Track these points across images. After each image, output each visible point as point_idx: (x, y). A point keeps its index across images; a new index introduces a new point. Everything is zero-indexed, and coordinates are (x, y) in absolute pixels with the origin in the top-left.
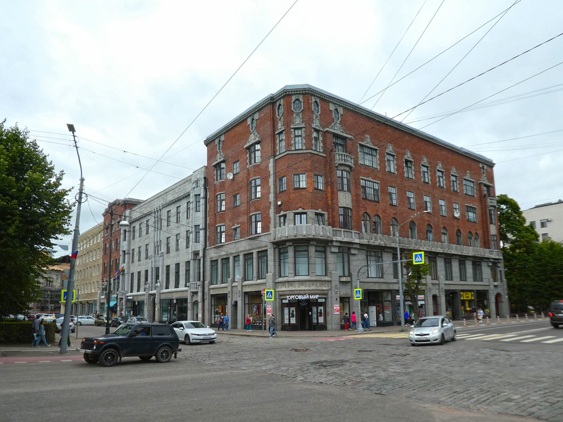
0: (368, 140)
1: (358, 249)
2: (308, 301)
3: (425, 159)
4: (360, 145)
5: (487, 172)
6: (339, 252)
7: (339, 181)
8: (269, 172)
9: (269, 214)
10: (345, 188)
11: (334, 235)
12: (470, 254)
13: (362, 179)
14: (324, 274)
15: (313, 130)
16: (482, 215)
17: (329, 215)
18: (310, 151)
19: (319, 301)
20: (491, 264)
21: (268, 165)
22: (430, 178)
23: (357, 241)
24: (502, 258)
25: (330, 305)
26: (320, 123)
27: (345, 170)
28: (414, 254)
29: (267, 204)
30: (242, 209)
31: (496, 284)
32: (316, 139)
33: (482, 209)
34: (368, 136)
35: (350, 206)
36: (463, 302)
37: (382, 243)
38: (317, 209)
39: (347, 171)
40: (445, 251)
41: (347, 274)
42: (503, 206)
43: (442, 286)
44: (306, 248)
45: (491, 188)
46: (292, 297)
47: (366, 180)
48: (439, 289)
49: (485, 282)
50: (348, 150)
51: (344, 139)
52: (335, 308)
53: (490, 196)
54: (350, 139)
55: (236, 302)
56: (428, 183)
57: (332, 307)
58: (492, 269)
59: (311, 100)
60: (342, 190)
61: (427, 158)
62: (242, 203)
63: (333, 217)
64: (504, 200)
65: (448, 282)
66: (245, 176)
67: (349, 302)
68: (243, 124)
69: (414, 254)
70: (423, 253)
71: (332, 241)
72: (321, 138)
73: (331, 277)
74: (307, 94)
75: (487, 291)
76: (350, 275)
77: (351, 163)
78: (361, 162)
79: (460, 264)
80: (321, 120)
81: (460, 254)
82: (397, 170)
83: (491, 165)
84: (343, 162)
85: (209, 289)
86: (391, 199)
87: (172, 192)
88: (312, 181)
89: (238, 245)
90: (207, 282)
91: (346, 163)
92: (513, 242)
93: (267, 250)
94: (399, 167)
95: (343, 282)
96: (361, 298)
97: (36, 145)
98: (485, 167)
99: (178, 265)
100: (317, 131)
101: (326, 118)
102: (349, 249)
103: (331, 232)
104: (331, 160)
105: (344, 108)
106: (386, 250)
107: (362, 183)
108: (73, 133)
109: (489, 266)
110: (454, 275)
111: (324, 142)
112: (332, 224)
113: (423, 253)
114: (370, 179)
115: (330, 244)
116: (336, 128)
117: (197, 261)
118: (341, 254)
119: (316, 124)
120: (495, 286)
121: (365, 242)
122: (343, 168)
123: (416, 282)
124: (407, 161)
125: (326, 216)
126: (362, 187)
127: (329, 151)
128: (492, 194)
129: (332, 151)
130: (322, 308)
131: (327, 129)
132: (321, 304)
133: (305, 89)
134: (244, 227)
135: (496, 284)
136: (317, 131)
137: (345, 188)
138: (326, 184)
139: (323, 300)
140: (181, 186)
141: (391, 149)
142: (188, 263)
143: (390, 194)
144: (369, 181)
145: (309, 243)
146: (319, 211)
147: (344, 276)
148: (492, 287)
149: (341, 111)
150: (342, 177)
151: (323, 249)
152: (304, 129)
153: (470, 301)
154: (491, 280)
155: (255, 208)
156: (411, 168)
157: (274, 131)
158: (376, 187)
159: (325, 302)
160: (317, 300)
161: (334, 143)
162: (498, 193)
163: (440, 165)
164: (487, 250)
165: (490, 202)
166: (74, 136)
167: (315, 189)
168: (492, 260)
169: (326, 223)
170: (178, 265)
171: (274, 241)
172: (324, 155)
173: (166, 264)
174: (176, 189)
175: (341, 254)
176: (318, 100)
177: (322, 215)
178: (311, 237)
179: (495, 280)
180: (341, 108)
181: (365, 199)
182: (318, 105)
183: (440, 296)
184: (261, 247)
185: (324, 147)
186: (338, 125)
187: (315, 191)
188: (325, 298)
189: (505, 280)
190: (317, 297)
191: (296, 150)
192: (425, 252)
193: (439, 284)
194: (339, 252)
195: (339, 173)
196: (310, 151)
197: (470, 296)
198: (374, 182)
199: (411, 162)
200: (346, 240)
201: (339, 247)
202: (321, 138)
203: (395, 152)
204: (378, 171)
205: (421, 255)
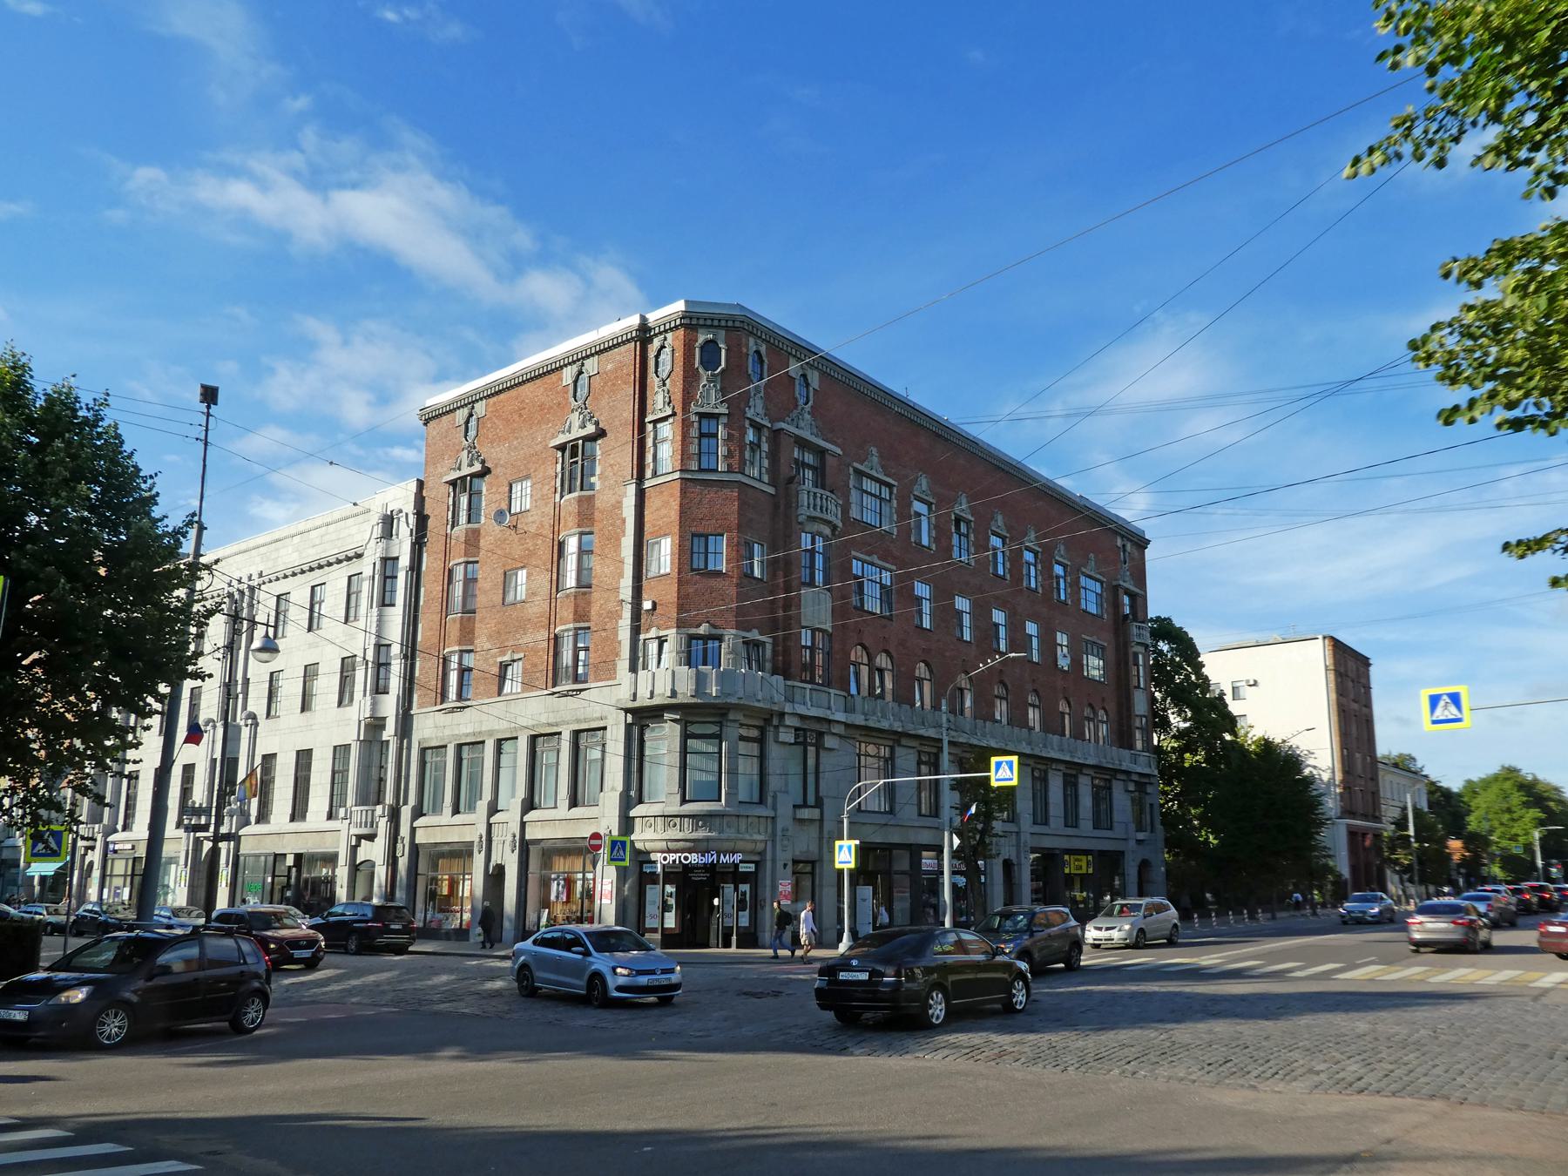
0: (875, 459)
1: (840, 736)
2: (710, 868)
3: (1000, 518)
4: (857, 471)
5: (1132, 559)
6: (796, 743)
7: (805, 561)
8: (624, 521)
9: (615, 631)
10: (819, 577)
11: (787, 700)
12: (1090, 762)
13: (858, 559)
14: (756, 798)
15: (747, 423)
16: (1118, 664)
17: (775, 644)
18: (739, 477)
19: (743, 868)
20: (1132, 787)
21: (620, 502)
22: (1008, 565)
23: (840, 716)
24: (1156, 772)
25: (768, 882)
26: (766, 408)
27: (820, 534)
28: (994, 760)
29: (611, 606)
30: (535, 609)
31: (1141, 836)
32: (755, 446)
33: (1117, 649)
34: (874, 450)
35: (828, 627)
36: (1069, 880)
37: (898, 727)
38: (749, 630)
39: (826, 539)
40: (1037, 752)
41: (811, 800)
42: (1164, 646)
43: (1025, 837)
44: (713, 729)
45: (1139, 600)
46: (671, 857)
47: (863, 562)
48: (1018, 845)
49: (1118, 831)
50: (828, 482)
51: (821, 453)
52: (781, 888)
53: (1135, 619)
54: (834, 455)
55: (500, 869)
56: (1003, 578)
57: (774, 887)
58: (1133, 800)
59: (747, 346)
60: (812, 584)
61: (970, 499)
62: (532, 593)
63: (786, 652)
64: (1164, 629)
65: (1037, 829)
66: (548, 522)
67: (812, 873)
68: (553, 377)
69: (994, 760)
70: (1015, 759)
71: (782, 715)
72: (765, 447)
73: (774, 808)
74: (736, 329)
75: (1122, 853)
76: (819, 803)
77: (834, 515)
78: (854, 513)
79: (1065, 784)
80: (767, 399)
81: (1068, 758)
82: (937, 540)
83: (1141, 543)
84: (817, 514)
85: (413, 830)
86: (920, 613)
87: (296, 539)
88: (743, 551)
89: (517, 708)
90: (406, 813)
91: (824, 516)
92: (1181, 734)
93: (605, 728)
94: (941, 534)
95: (802, 821)
96: (852, 865)
97: (118, 436)
98: (1129, 546)
99: (304, 759)
100: (758, 427)
101: (782, 397)
102: (820, 735)
103: (782, 690)
104: (788, 506)
105: (823, 374)
106: (904, 741)
107: (856, 567)
108: (208, 407)
109: (1127, 791)
110: (1117, 817)
111: (774, 456)
112: (783, 669)
113: (1015, 759)
114: (875, 559)
115: (775, 722)
116: (802, 424)
117: (376, 748)
118: (799, 749)
119: (756, 410)
120: (1139, 842)
121: (859, 720)
122: (816, 527)
123: (980, 826)
124: (958, 520)
125: (769, 648)
126: (856, 577)
127: (785, 484)
128: (1140, 615)
129: (791, 480)
130: (745, 888)
131: (783, 425)
132: (745, 878)
133: (733, 318)
134: (535, 660)
135: (1141, 836)
136: (758, 427)
137: (819, 577)
138: (771, 566)
139: (751, 868)
140: (331, 528)
141: (760, 409)
142: (341, 751)
143: (919, 600)
144: (873, 564)
145: (724, 715)
146: (755, 635)
147: (805, 805)
148: (1132, 843)
149: (814, 379)
150: (812, 552)
151: (754, 733)
152: (724, 420)
153: (1083, 877)
154: (1133, 827)
155: (576, 612)
156: (967, 536)
157: (643, 412)
158: (886, 578)
159: (756, 873)
160: (736, 866)
161: (796, 461)
162: (1151, 614)
163: (924, 482)
164: (1126, 753)
165: (1139, 634)
166: (208, 415)
167: (746, 575)
168: (1135, 778)
169: (768, 665)
170: (304, 759)
171: (631, 705)
172: (771, 490)
173: (261, 751)
174: (314, 534)
175: (799, 749)
176: (763, 349)
177: (758, 644)
178: (733, 700)
179: (1140, 829)
180: (816, 374)
181: (861, 609)
182: (762, 362)
183: (1020, 864)
184: (585, 721)
185: (774, 471)
186: (807, 417)
187: (745, 581)
188: (756, 863)
189: (1159, 827)
190: (738, 857)
191: (701, 470)
192: (1020, 755)
193: (1018, 833)
194: (796, 743)
195: (806, 540)
196: (739, 477)
197: (1084, 865)
198: (882, 568)
199: (968, 522)
200: (813, 712)
201: (797, 729)
202: (765, 447)
203: (935, 495)
204: (893, 541)
205: (1010, 764)
